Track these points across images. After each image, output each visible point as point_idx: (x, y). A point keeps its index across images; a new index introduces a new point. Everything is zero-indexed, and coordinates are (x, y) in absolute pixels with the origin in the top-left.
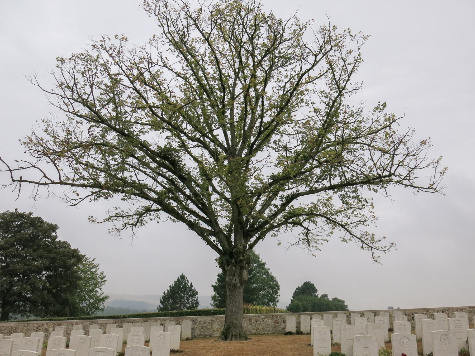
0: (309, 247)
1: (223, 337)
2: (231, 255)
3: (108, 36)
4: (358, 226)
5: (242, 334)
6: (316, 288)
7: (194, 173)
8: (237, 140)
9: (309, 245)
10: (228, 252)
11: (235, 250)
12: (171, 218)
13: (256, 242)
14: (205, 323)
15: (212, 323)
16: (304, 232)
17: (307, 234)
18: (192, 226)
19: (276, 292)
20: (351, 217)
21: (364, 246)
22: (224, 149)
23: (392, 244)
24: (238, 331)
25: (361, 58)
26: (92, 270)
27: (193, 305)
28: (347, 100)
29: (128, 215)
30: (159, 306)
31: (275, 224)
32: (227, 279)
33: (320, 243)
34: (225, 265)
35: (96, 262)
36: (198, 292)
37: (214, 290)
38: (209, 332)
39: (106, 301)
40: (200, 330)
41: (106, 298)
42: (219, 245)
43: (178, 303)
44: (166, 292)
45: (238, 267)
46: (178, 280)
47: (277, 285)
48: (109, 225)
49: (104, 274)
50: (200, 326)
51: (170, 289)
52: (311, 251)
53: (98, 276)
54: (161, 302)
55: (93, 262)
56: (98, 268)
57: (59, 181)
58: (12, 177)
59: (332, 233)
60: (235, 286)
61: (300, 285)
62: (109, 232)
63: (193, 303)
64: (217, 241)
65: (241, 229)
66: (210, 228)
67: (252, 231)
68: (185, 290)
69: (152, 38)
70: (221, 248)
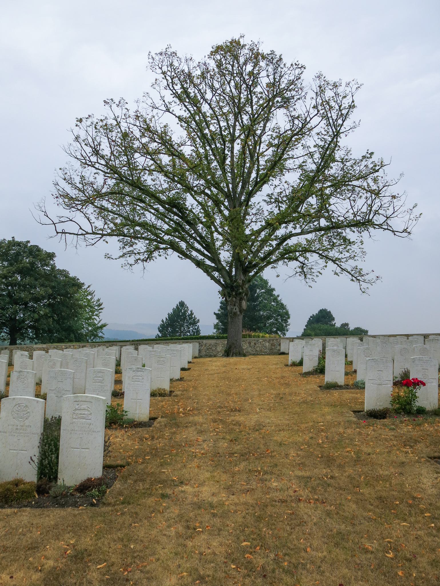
1: (226, 354)
2: (232, 288)
4: (349, 261)
5: (241, 352)
6: (334, 316)
7: (197, 209)
8: (238, 180)
10: (229, 286)
12: (179, 256)
14: (210, 345)
15: (216, 345)
16: (300, 266)
17: (302, 268)
18: (199, 264)
19: (286, 321)
21: (354, 279)
22: (225, 194)
23: (378, 277)
24: (237, 350)
25: (354, 105)
26: (88, 297)
27: (194, 333)
28: (342, 141)
29: (139, 252)
30: (158, 335)
31: (272, 260)
32: (229, 308)
33: (315, 275)
35: (91, 289)
36: (199, 320)
37: (217, 319)
38: (214, 353)
39: (104, 328)
40: (206, 351)
41: (104, 325)
42: (222, 280)
43: (178, 332)
44: (165, 320)
46: (177, 307)
47: (287, 313)
48: (122, 260)
49: (101, 301)
50: (205, 347)
51: (169, 317)
52: (307, 283)
53: (95, 303)
54: (160, 331)
55: (88, 289)
56: (93, 295)
57: (91, 232)
58: (56, 230)
59: (326, 266)
60: (235, 314)
61: (315, 312)
62: (122, 267)
63: (194, 332)
64: (220, 277)
65: (241, 266)
66: (213, 265)
67: (250, 267)
68: (185, 318)
69: (154, 81)
70: (223, 283)
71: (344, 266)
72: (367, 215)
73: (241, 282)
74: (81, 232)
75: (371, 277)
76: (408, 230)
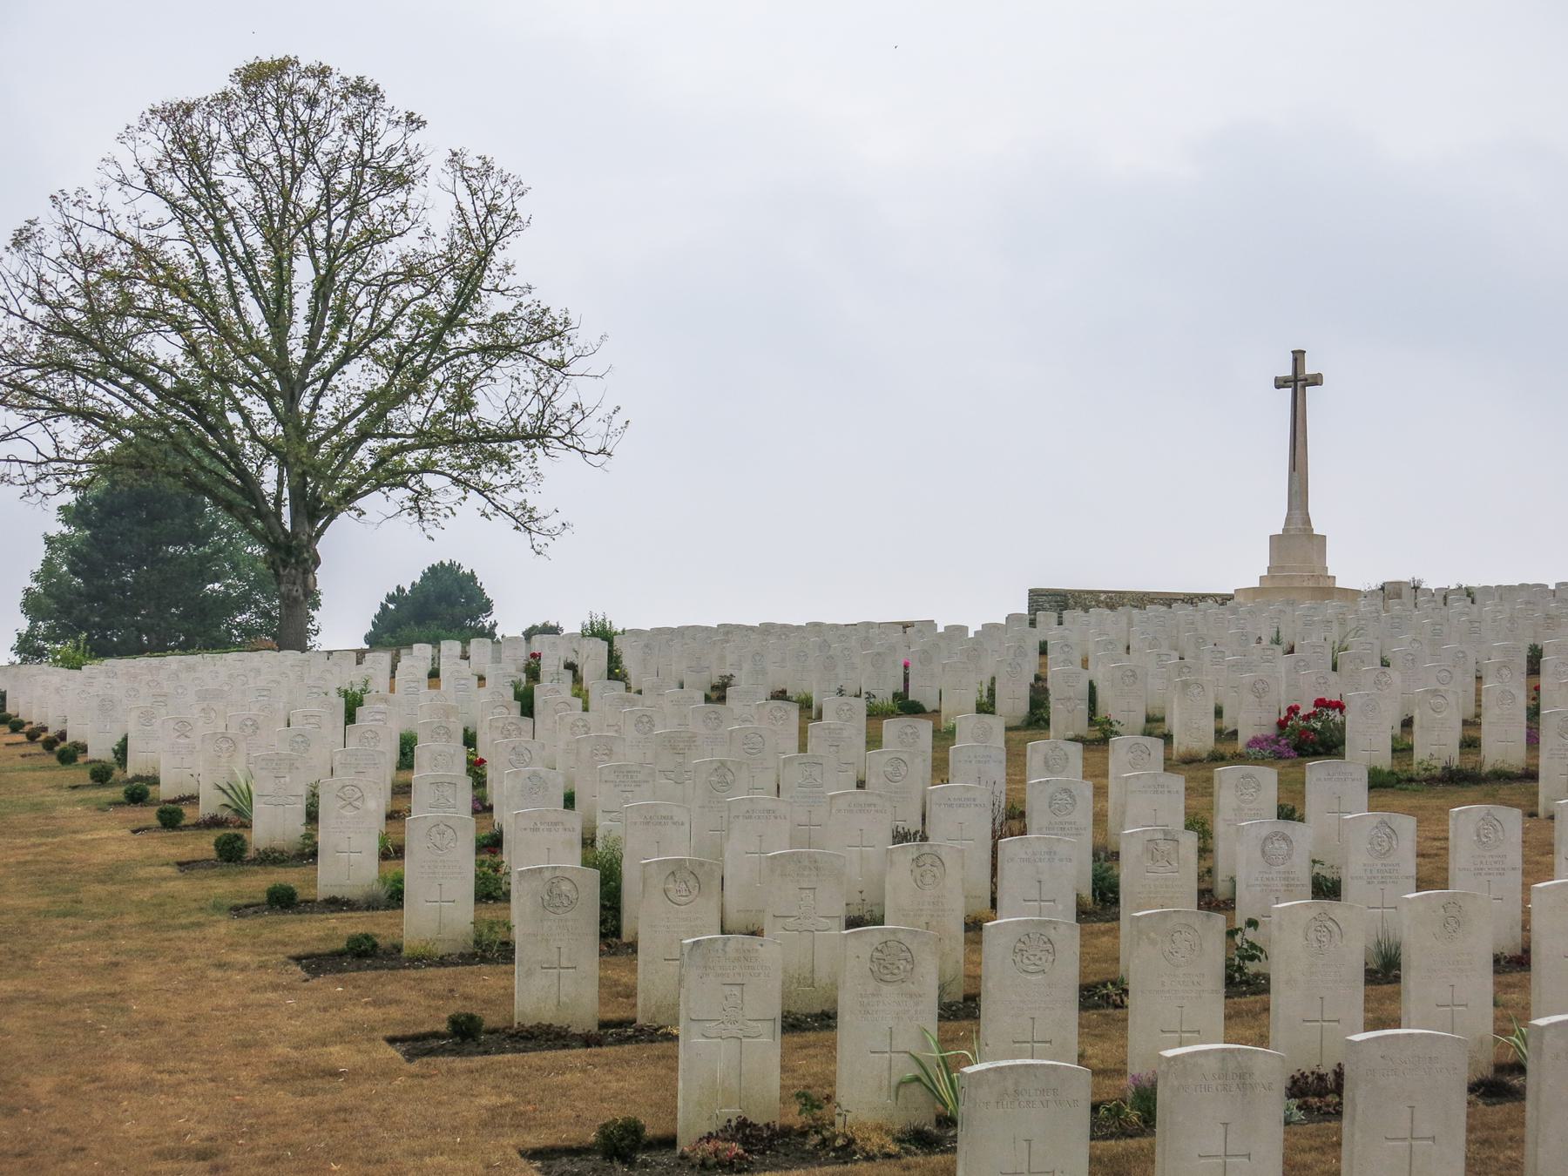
6: (488, 594)
9: (421, 518)
13: (325, 526)
21: (519, 525)
45: (300, 570)
59: (464, 499)
71: (499, 500)
73: (305, 538)
76: (608, 450)
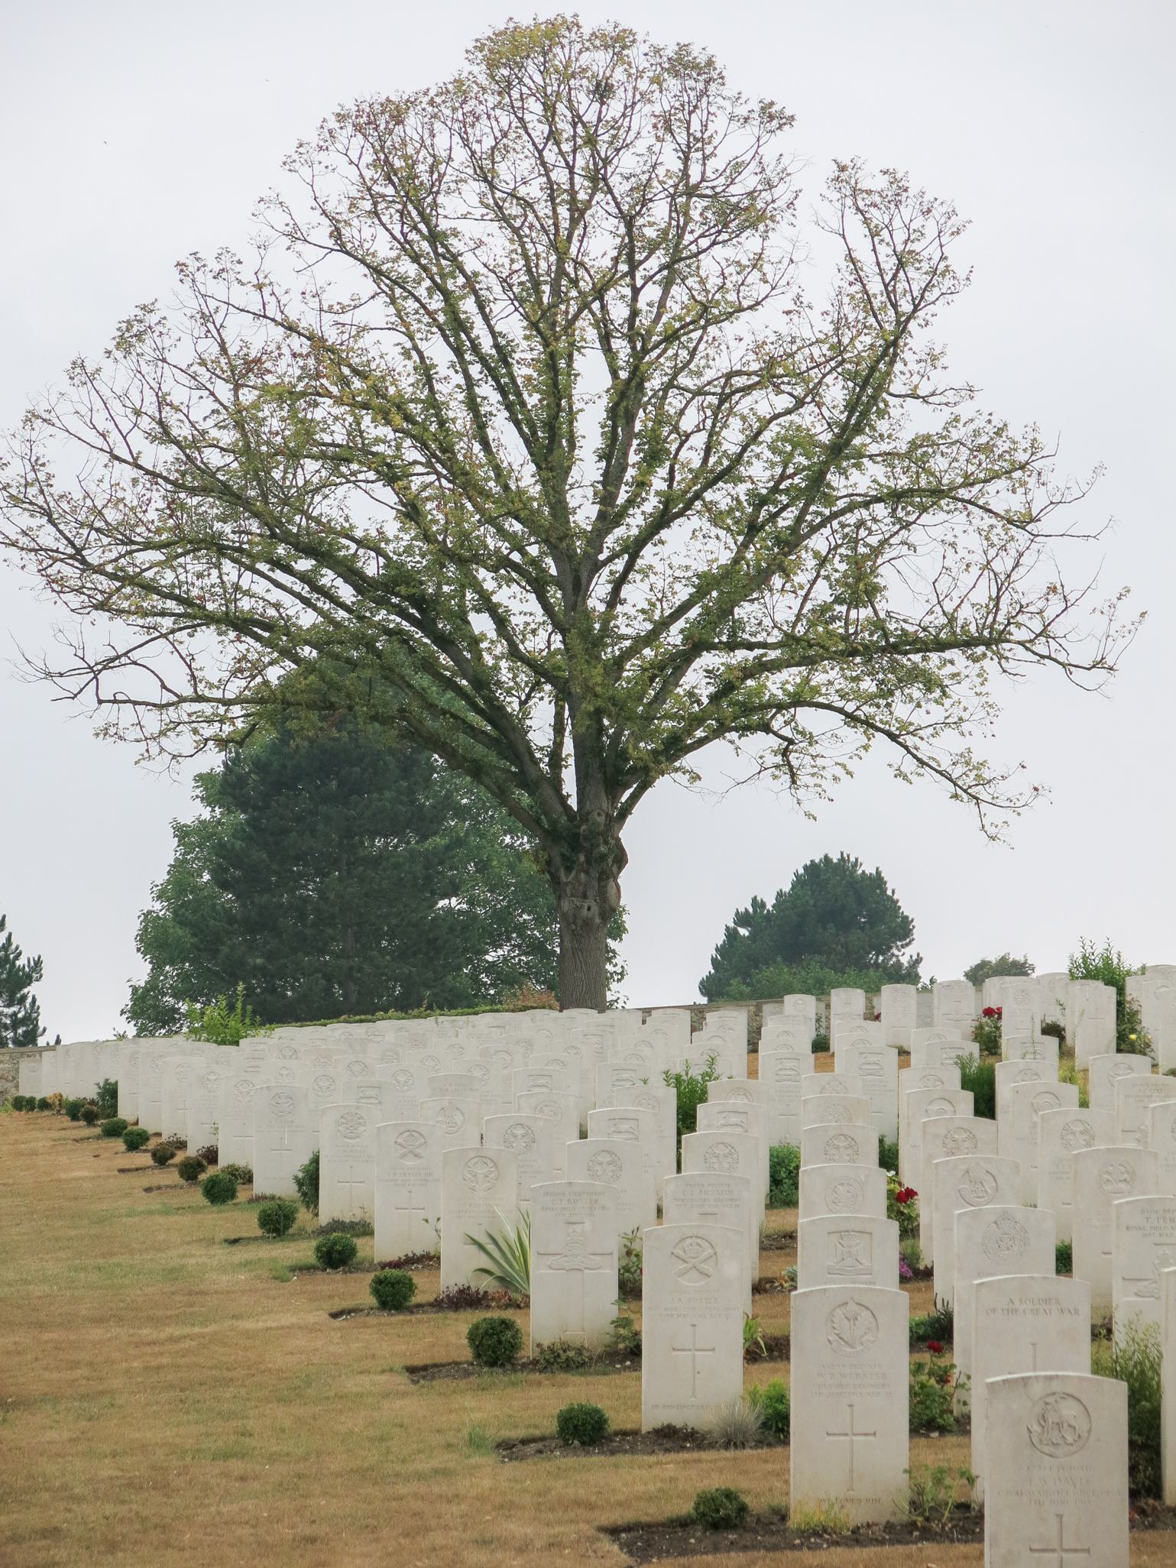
0: (793, 791)
3: (238, 276)
6: (907, 908)
11: (583, 827)
17: (785, 753)
20: (922, 703)
21: (959, 792)
34: (558, 870)
45: (595, 874)
59: (866, 748)
72: (988, 614)
73: (601, 819)
74: (168, 697)
75: (1015, 787)
76: (1110, 662)
